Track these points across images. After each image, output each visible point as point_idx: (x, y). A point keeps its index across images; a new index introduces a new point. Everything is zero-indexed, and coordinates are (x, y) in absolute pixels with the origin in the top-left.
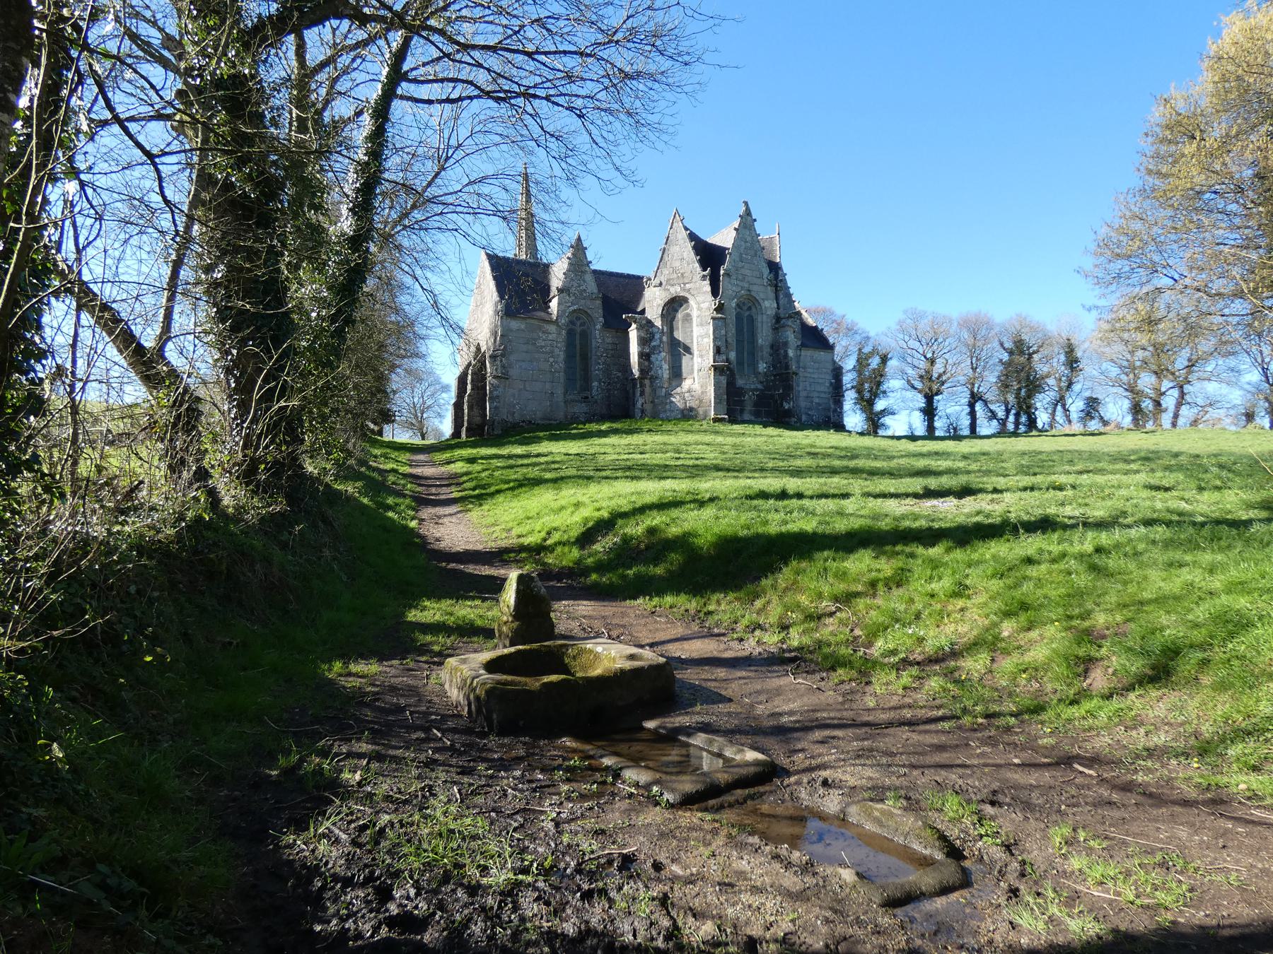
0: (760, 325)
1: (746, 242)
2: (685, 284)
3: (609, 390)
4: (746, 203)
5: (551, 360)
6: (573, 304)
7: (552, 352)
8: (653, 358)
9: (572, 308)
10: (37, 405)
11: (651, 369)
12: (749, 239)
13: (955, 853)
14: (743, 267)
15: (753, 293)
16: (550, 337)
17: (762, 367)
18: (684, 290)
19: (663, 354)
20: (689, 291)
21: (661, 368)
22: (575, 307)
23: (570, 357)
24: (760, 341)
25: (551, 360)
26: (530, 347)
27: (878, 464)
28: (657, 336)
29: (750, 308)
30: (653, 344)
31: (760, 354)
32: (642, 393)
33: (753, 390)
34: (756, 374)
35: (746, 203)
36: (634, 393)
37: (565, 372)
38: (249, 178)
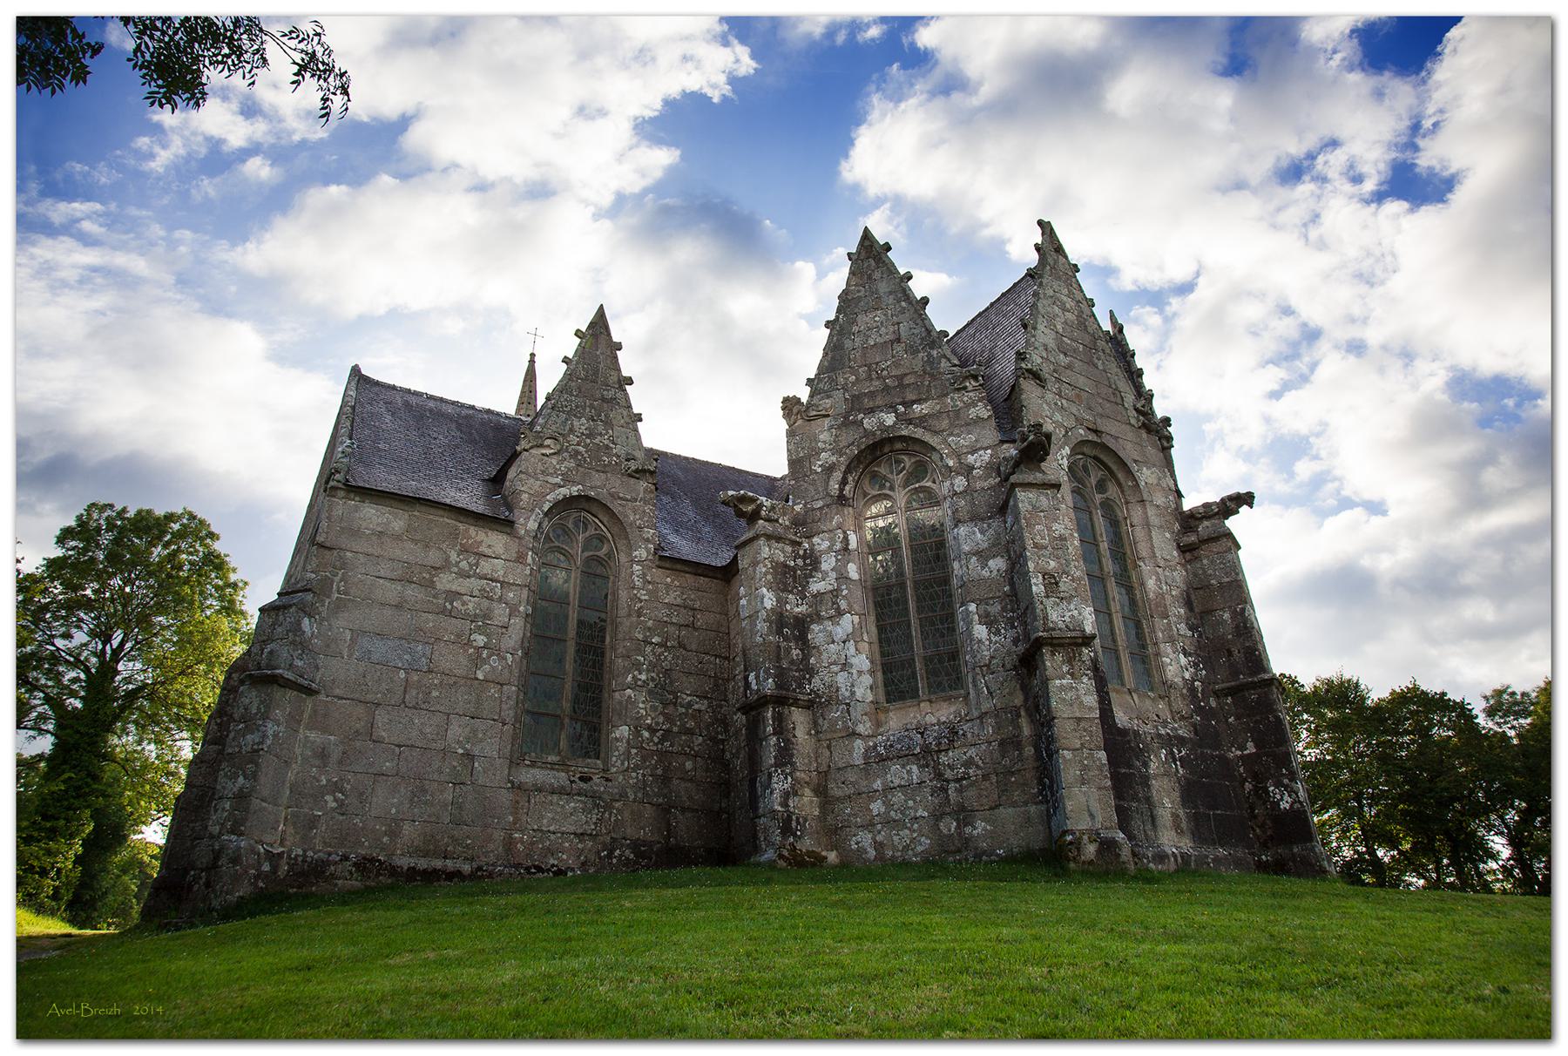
0: (1140, 533)
1: (1064, 310)
2: (908, 404)
3: (663, 755)
4: (1044, 226)
5: (480, 640)
6: (567, 481)
7: (487, 616)
8: (816, 633)
9: (564, 491)
10: (104, 870)
11: (812, 672)
12: (1070, 304)
13: (321, 546)
14: (1069, 367)
15: (1106, 440)
16: (485, 567)
17: (1176, 665)
18: (910, 421)
19: (848, 623)
20: (922, 421)
21: (846, 666)
22: (575, 490)
23: (449, 511)
24: (1151, 583)
25: (480, 640)
26: (412, 593)
27: (438, 863)
28: (828, 563)
29: (1101, 487)
30: (817, 586)
31: (1160, 623)
32: (785, 757)
33: (1170, 741)
34: (1165, 690)
35: (1044, 226)
36: (754, 761)
37: (524, 687)
38: (648, 671)
